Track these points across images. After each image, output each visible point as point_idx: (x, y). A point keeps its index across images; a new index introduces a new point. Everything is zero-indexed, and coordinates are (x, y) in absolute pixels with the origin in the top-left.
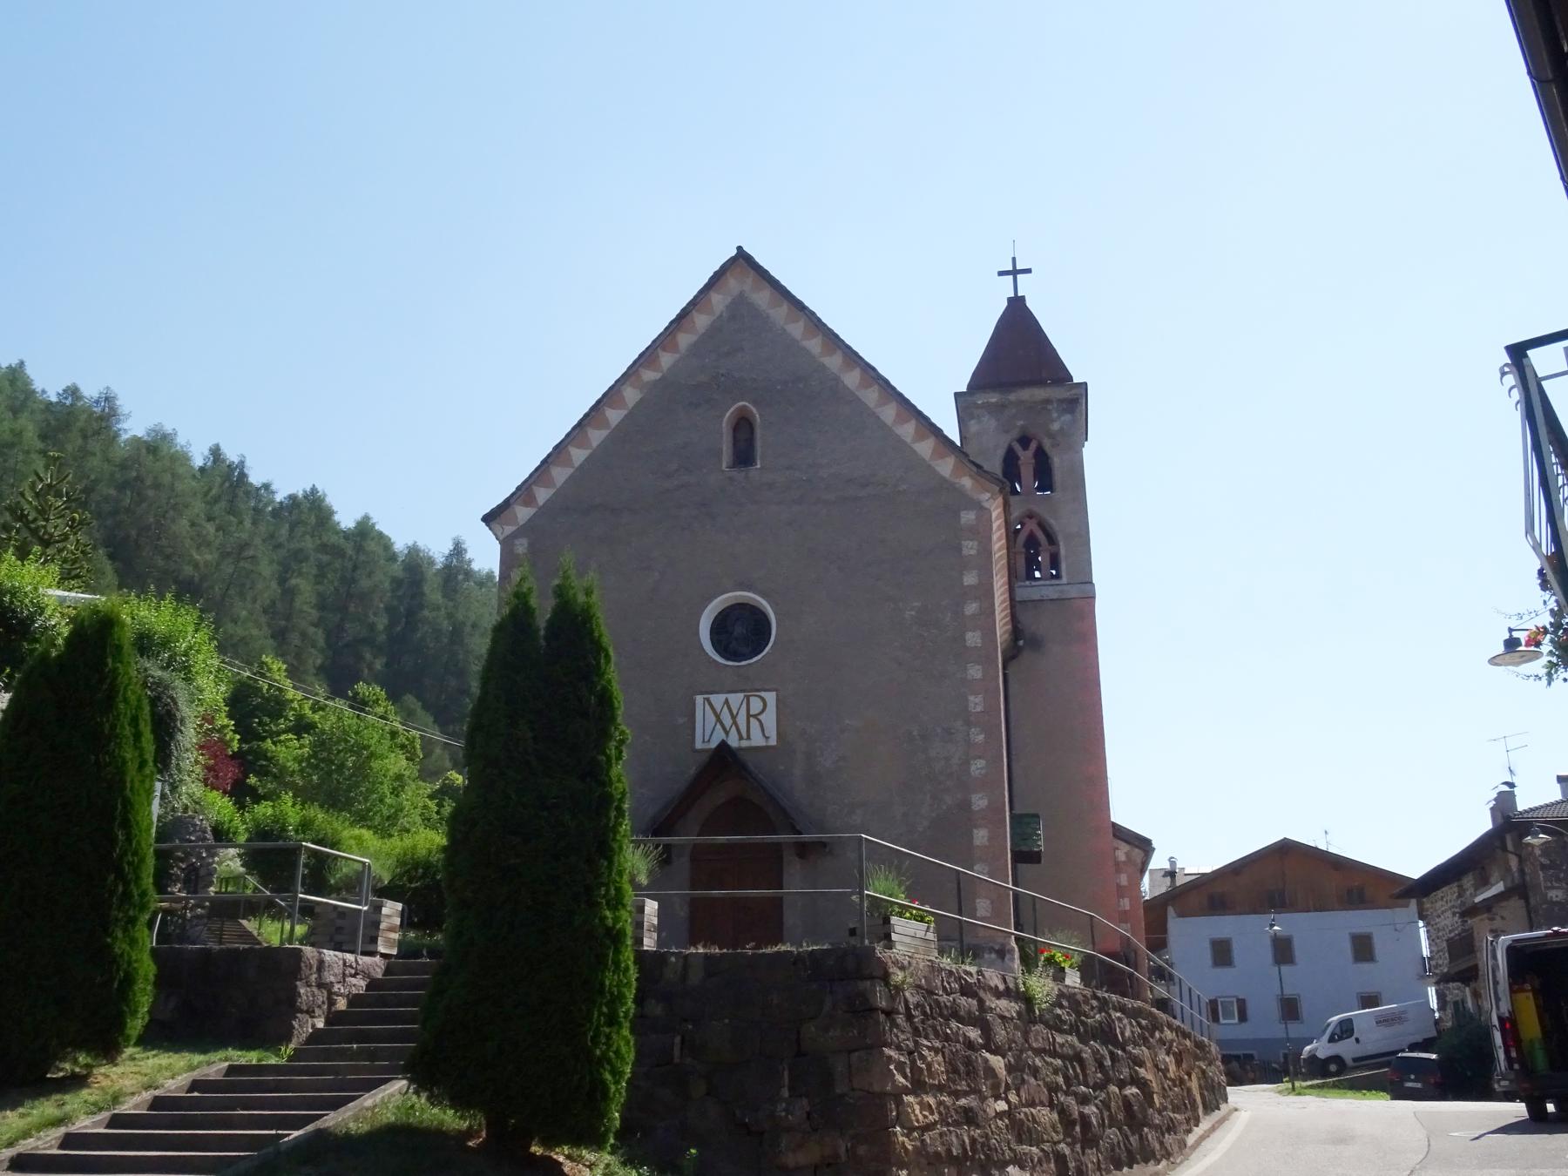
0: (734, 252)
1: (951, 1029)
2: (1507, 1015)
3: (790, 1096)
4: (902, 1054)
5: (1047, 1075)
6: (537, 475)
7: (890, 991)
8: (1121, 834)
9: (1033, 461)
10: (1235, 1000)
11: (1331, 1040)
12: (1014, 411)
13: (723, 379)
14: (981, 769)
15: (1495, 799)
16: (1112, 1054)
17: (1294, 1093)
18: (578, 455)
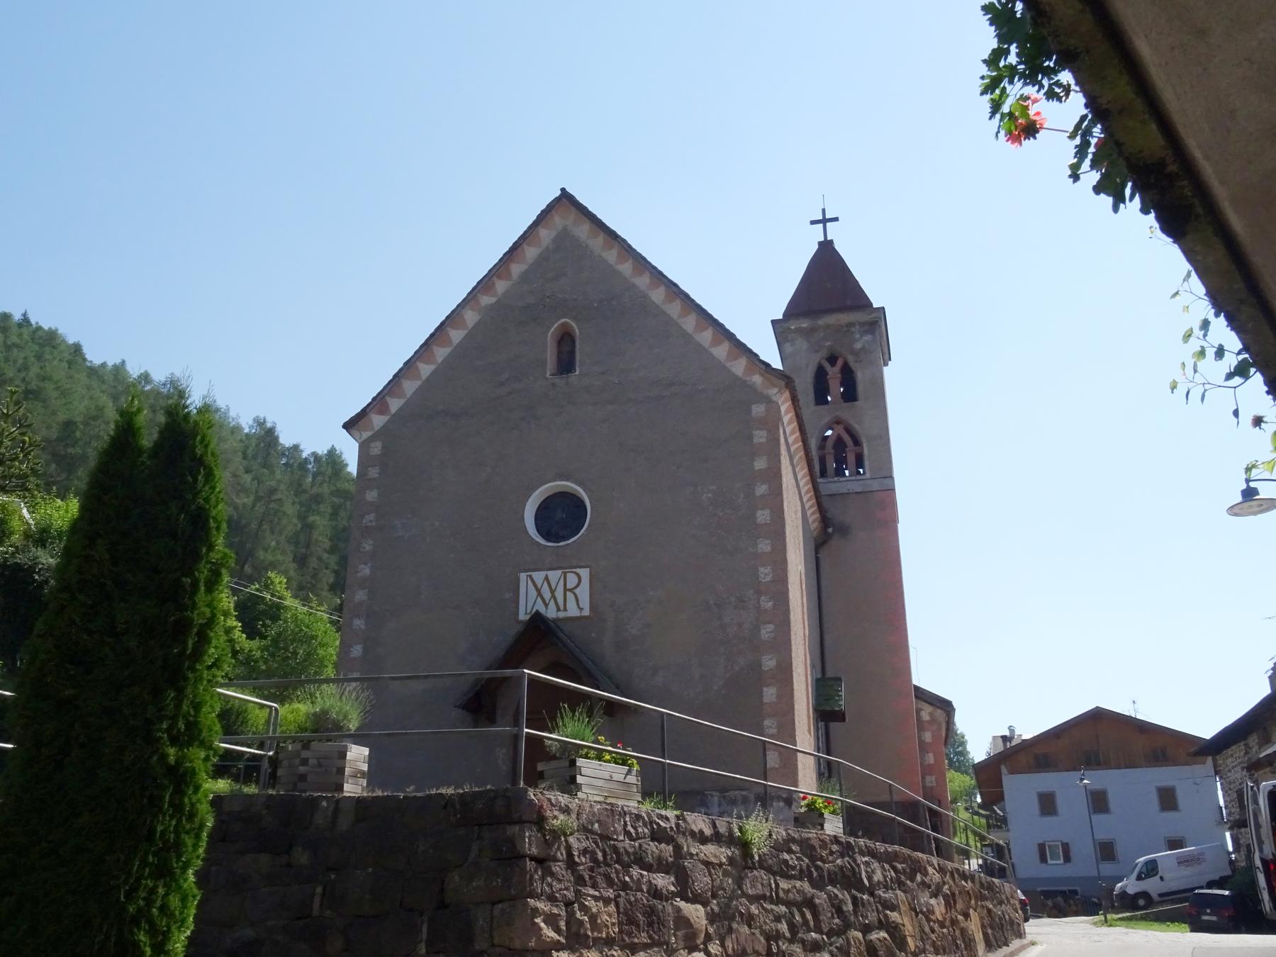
0: (559, 193)
1: (631, 877)
2: (1271, 857)
3: (427, 952)
4: (557, 906)
5: (765, 922)
6: (390, 386)
7: (544, 836)
8: (922, 695)
9: (840, 375)
10: (1059, 843)
11: (1139, 878)
12: (822, 334)
13: (548, 300)
14: (771, 632)
15: (1273, 669)
16: (854, 899)
17: (1105, 925)
18: (426, 370)
